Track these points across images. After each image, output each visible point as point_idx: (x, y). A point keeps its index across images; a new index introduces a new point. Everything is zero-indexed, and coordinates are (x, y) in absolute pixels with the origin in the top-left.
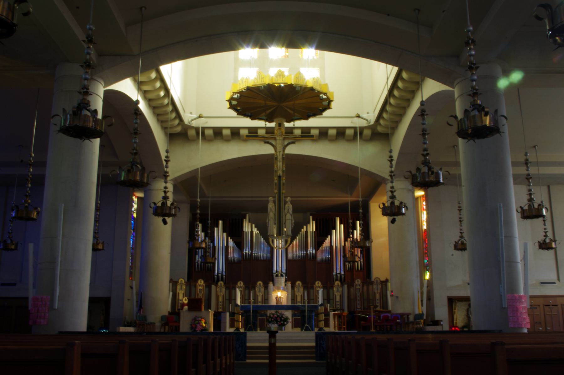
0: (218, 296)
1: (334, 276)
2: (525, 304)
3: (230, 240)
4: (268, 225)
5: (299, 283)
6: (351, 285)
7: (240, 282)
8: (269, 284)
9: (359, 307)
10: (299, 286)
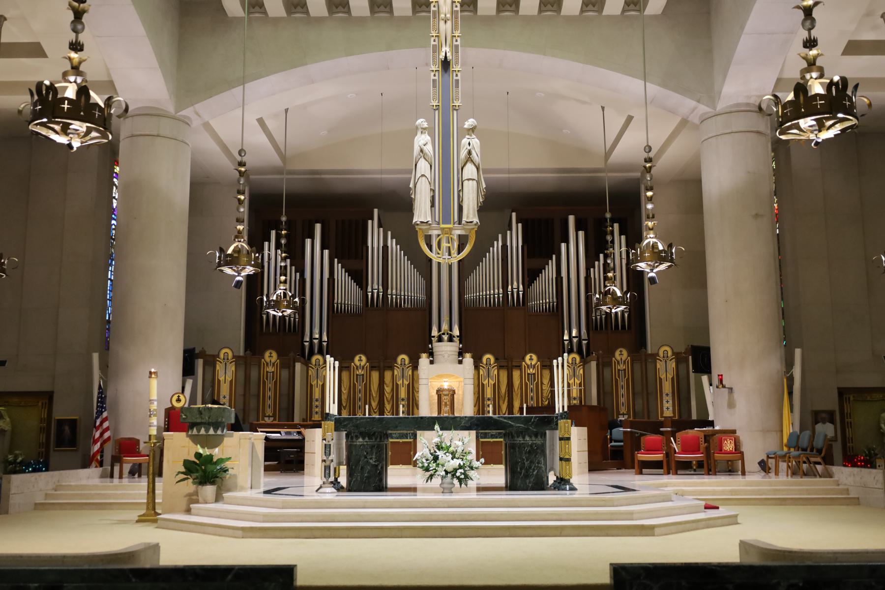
0: (311, 386)
1: (566, 343)
2: (271, 315)
3: (338, 267)
4: (413, 203)
5: (488, 357)
6: (604, 364)
7: (620, 350)
8: (420, 360)
9: (623, 410)
10: (488, 363)
